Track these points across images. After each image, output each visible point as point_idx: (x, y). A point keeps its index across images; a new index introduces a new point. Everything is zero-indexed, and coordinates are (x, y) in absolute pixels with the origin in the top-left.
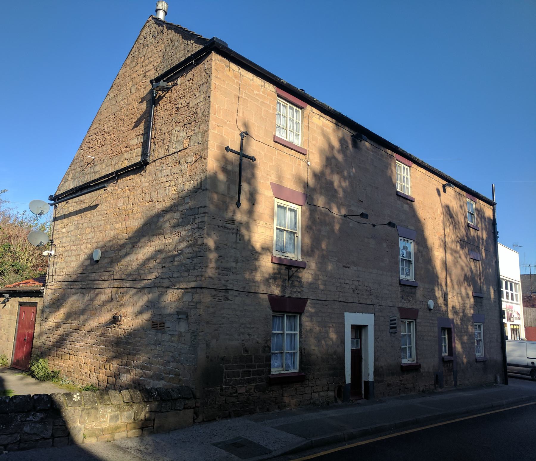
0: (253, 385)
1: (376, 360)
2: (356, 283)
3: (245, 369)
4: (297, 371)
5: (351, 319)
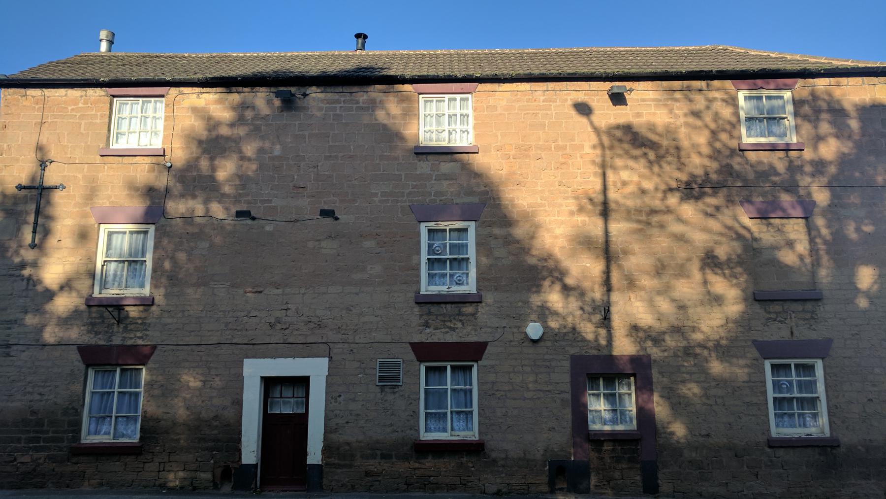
0: (43, 454)
3: (32, 435)
4: (136, 441)
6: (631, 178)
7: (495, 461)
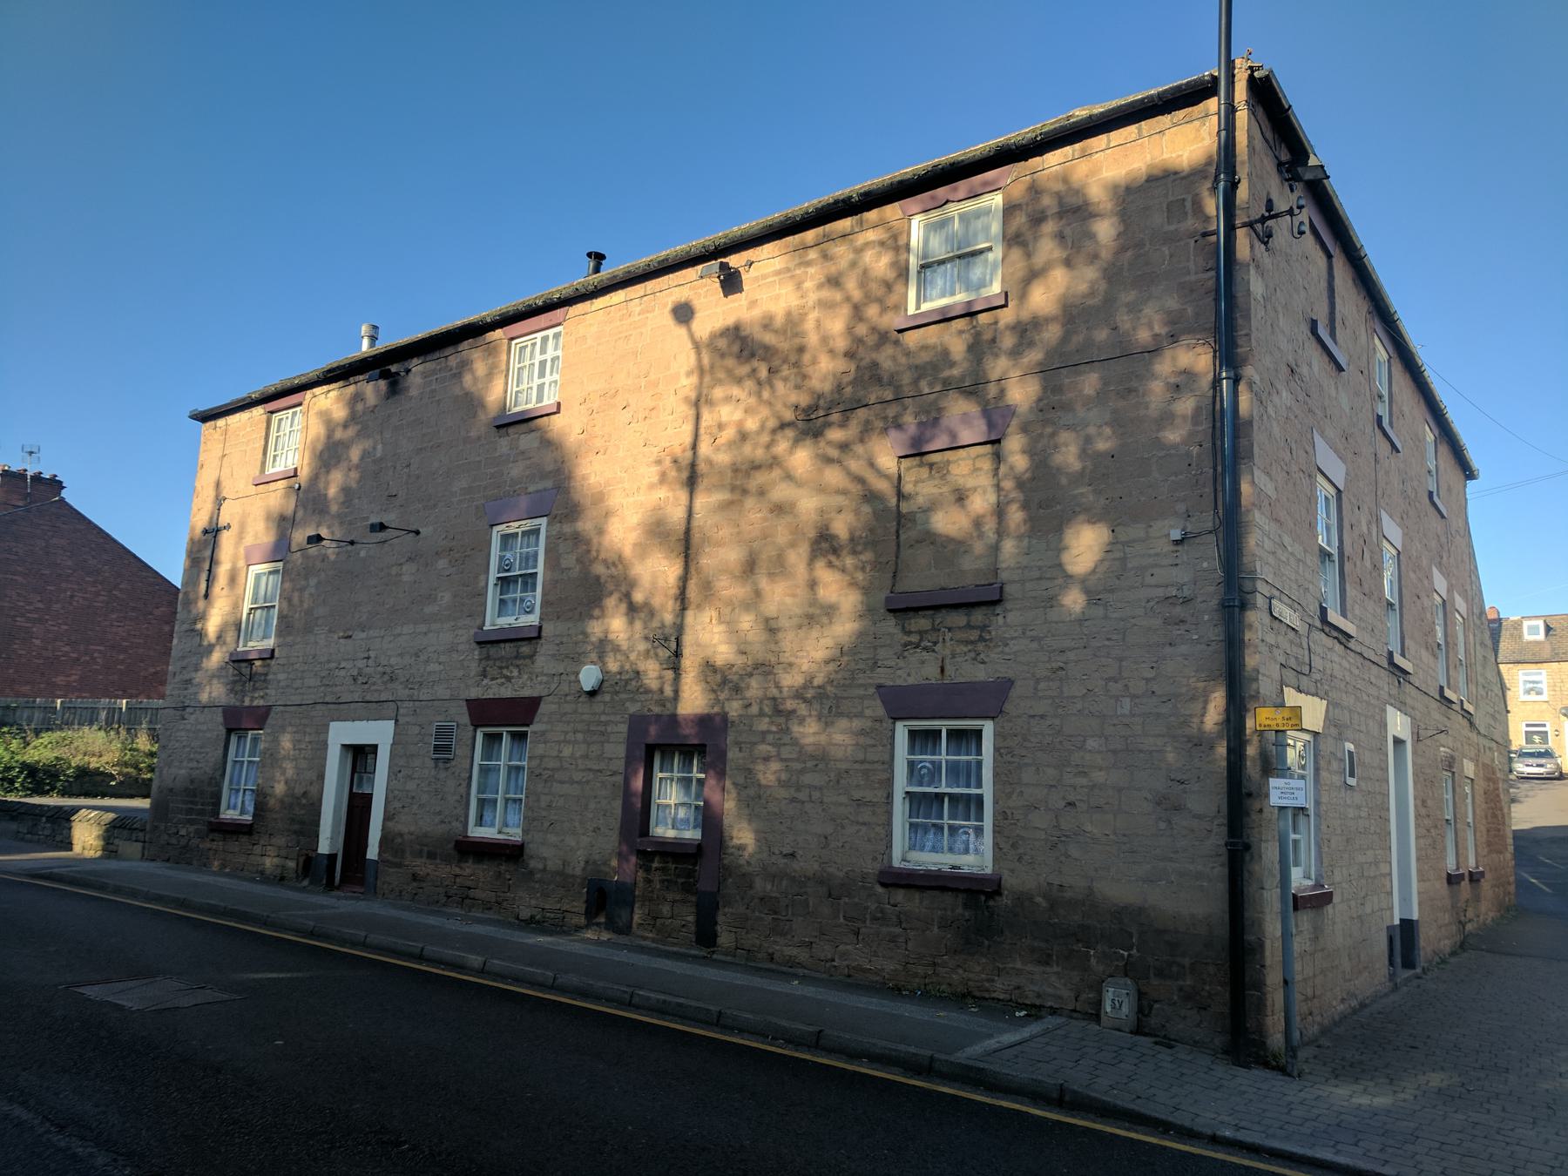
0: (192, 829)
1: (388, 817)
2: (361, 664)
4: (248, 818)
5: (343, 733)
6: (736, 411)
7: (531, 873)
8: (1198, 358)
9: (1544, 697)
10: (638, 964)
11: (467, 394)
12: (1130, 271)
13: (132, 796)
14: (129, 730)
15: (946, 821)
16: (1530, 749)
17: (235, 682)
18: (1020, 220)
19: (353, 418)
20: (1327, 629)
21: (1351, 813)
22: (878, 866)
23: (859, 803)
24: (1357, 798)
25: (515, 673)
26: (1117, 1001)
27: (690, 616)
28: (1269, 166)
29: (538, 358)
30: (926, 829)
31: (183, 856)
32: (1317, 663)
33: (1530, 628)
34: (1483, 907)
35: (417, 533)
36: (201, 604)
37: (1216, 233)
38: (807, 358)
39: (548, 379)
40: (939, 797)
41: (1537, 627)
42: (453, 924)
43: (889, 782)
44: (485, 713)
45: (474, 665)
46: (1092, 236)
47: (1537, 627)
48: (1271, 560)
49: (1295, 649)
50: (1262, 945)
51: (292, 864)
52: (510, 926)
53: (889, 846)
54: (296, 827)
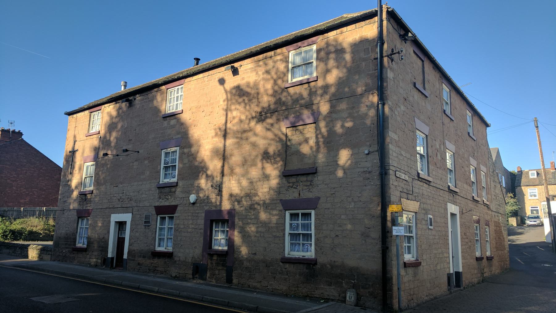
0: (67, 250)
1: (130, 245)
2: (121, 195)
4: (85, 246)
5: (115, 218)
6: (238, 113)
7: (176, 262)
8: (375, 99)
9: (537, 198)
10: (209, 288)
11: (156, 107)
12: (353, 71)
13: (47, 241)
14: (46, 218)
15: (301, 242)
16: (533, 216)
17: (80, 202)
18: (322, 54)
19: (119, 114)
20: (421, 180)
21: (431, 237)
22: (281, 256)
23: (275, 237)
24: (434, 232)
25: (170, 197)
26: (351, 296)
27: (226, 179)
28: (396, 36)
29: (176, 95)
30: (295, 244)
31: (64, 259)
32: (416, 190)
33: (531, 174)
34: (494, 268)
35: (138, 152)
36: (70, 176)
37: (377, 59)
38: (260, 96)
39: (179, 102)
40: (300, 234)
41: (534, 173)
42: (151, 278)
43: (284, 230)
44: (160, 210)
45: (157, 195)
46: (344, 59)
47: (534, 173)
48: (396, 159)
49: (406, 186)
50: (392, 278)
51: (99, 261)
52: (169, 279)
53: (284, 250)
54: (101, 249)
